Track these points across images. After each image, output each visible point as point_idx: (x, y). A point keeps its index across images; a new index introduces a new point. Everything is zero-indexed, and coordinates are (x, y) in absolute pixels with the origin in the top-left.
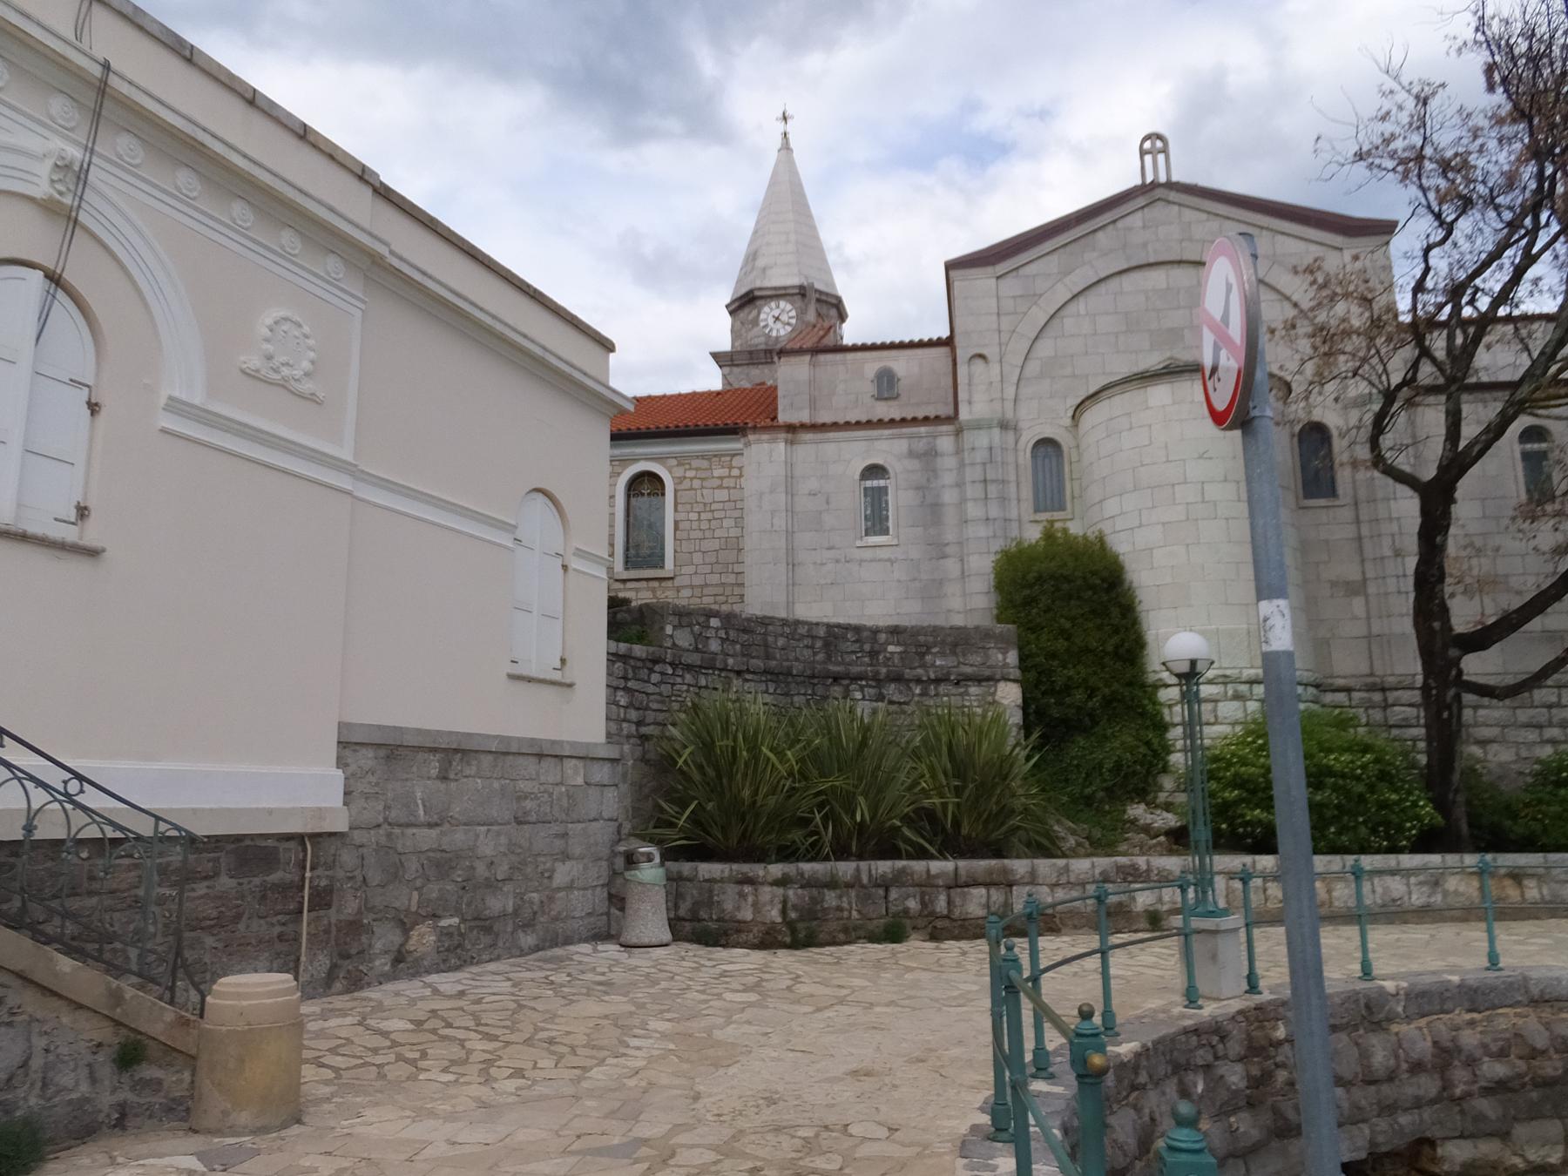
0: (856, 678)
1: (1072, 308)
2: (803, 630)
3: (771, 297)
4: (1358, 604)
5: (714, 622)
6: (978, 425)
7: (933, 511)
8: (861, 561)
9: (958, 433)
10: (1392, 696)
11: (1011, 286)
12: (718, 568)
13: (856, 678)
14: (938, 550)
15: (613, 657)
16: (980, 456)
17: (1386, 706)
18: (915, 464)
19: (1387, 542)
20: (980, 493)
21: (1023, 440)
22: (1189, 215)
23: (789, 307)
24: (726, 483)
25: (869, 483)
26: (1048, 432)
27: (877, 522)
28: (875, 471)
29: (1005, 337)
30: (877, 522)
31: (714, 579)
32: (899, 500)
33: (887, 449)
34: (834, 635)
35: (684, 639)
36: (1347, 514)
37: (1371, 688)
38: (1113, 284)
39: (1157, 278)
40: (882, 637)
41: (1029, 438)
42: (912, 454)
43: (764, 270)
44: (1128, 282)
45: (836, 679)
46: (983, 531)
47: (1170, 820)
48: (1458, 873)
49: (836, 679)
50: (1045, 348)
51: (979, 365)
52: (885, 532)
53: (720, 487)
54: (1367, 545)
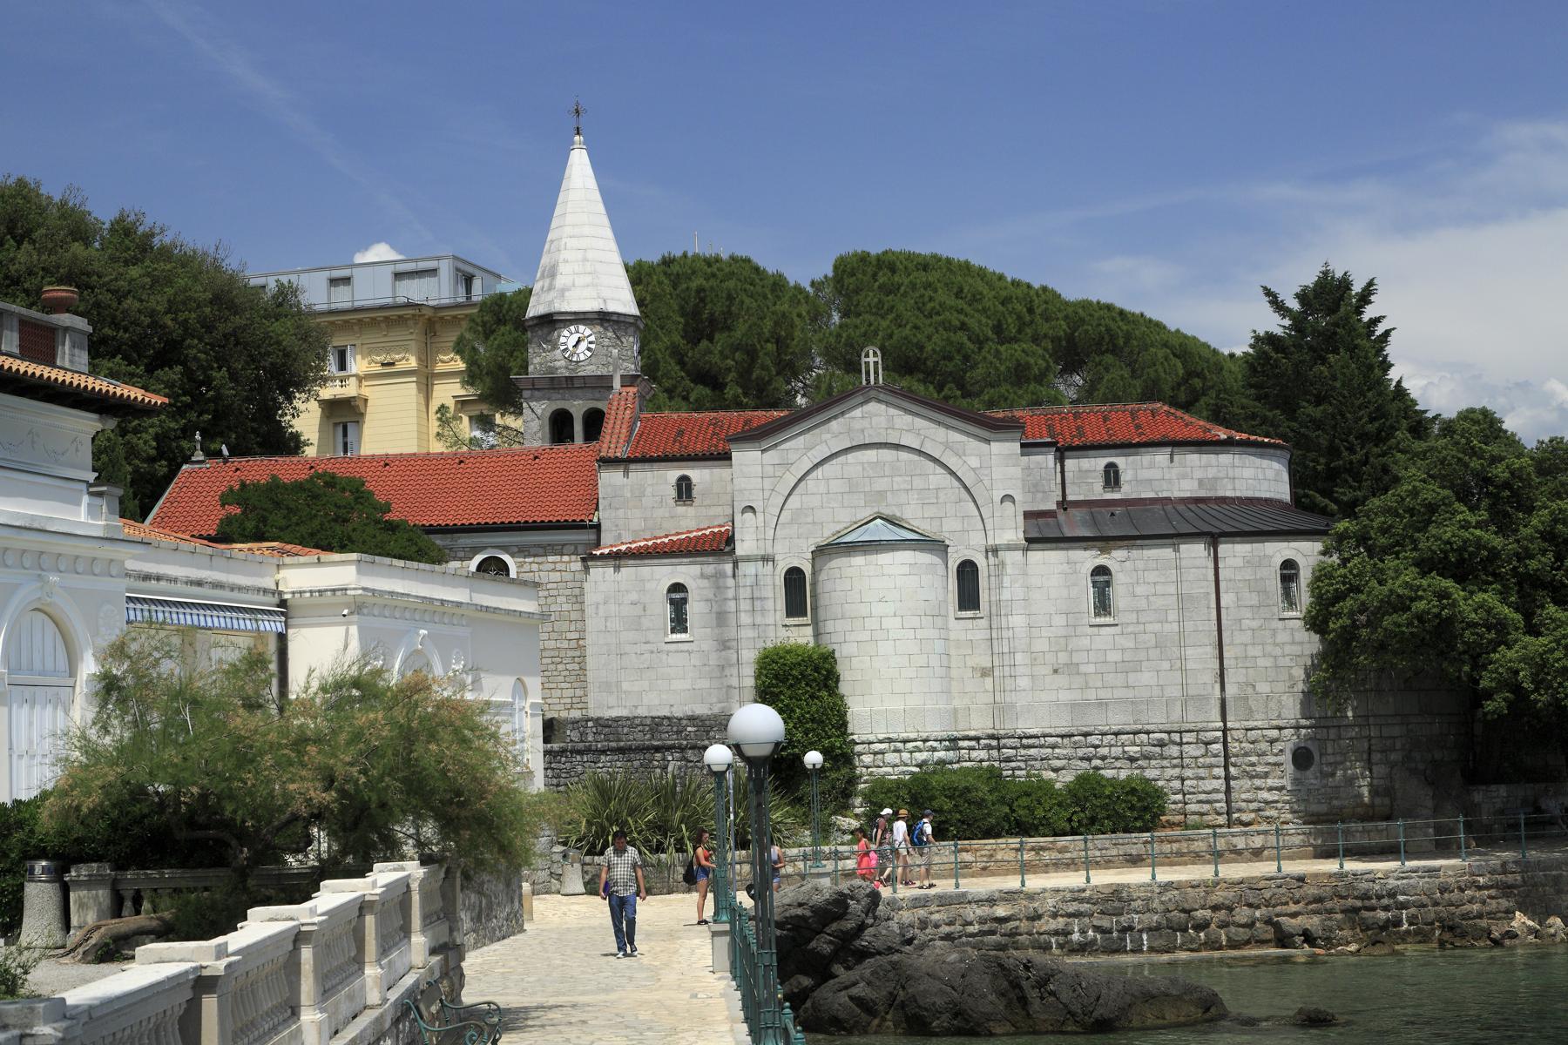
0: (669, 748)
1: (814, 474)
2: (637, 722)
3: (572, 322)
4: (989, 680)
5: (590, 724)
6: (748, 559)
7: (721, 618)
8: (668, 653)
9: (735, 564)
10: (1003, 741)
11: (772, 456)
12: (554, 636)
13: (669, 748)
14: (724, 645)
15: (546, 753)
16: (749, 581)
17: (999, 748)
18: (705, 583)
19: (1005, 642)
20: (749, 607)
21: (779, 568)
22: (892, 411)
23: (588, 332)
24: (558, 567)
25: (674, 596)
26: (796, 564)
27: (679, 623)
28: (677, 588)
29: (767, 494)
30: (679, 623)
31: (552, 644)
32: (694, 609)
33: (686, 572)
34: (656, 724)
35: (575, 736)
36: (984, 623)
37: (992, 737)
38: (842, 459)
39: (871, 454)
40: (684, 722)
41: (783, 567)
42: (703, 576)
43: (563, 291)
44: (851, 457)
45: (657, 749)
46: (750, 633)
47: (855, 824)
48: (1005, 847)
49: (657, 749)
50: (794, 502)
51: (749, 515)
52: (685, 630)
53: (554, 570)
54: (995, 643)
